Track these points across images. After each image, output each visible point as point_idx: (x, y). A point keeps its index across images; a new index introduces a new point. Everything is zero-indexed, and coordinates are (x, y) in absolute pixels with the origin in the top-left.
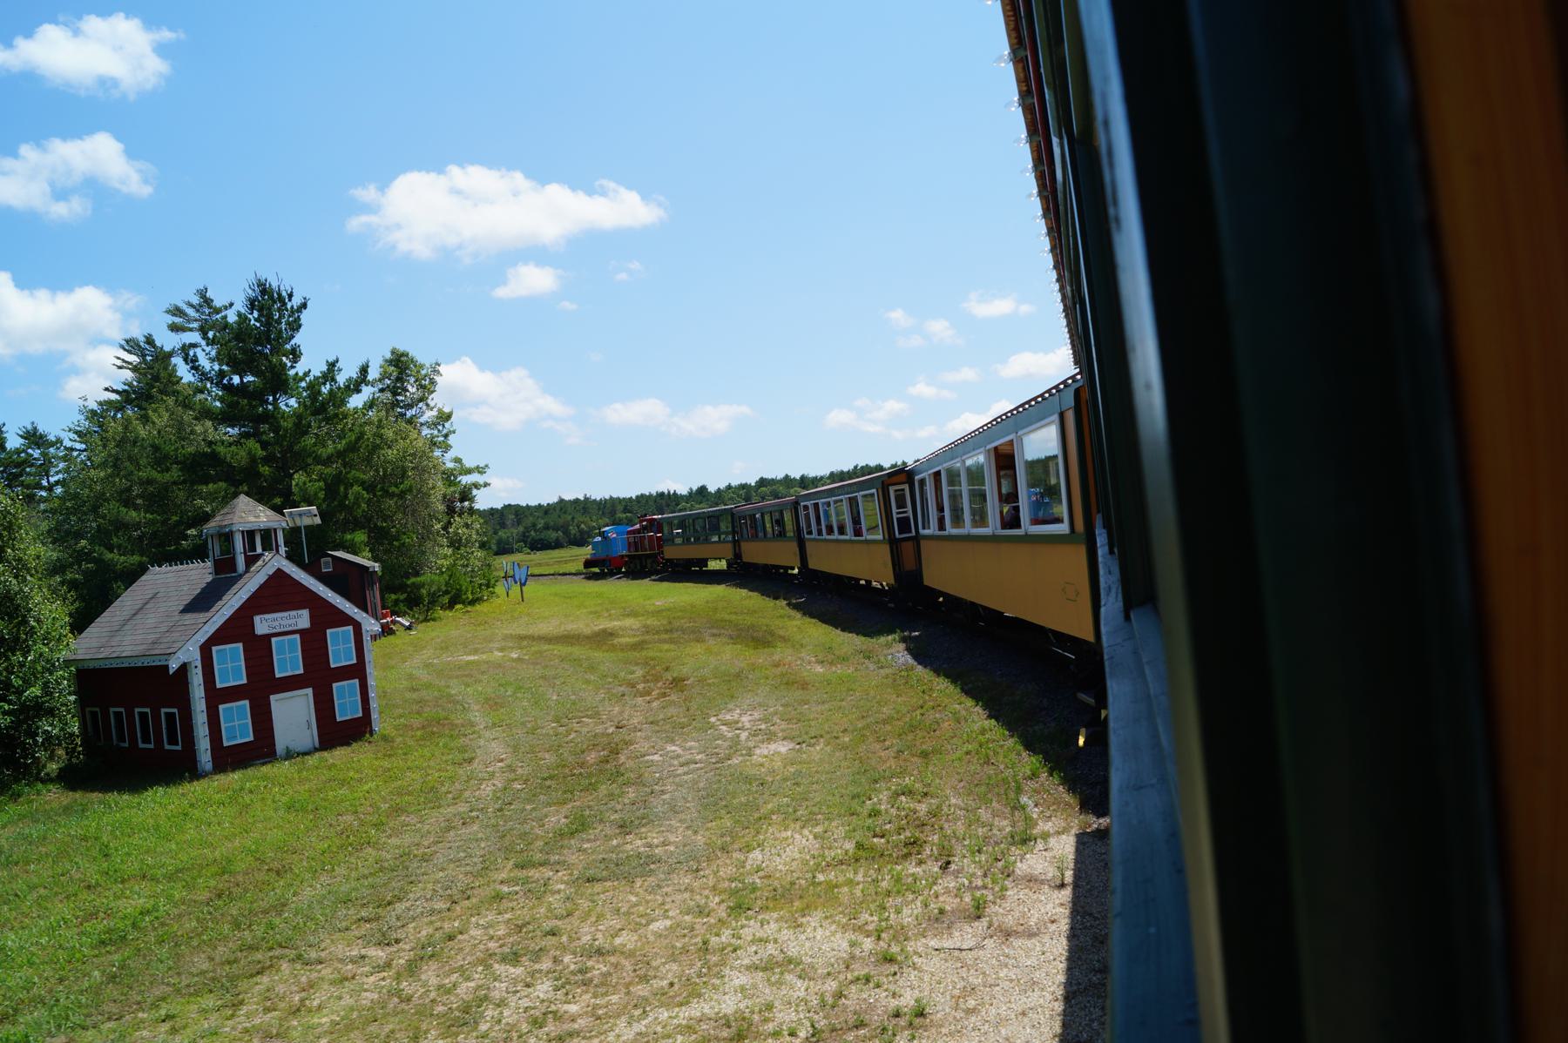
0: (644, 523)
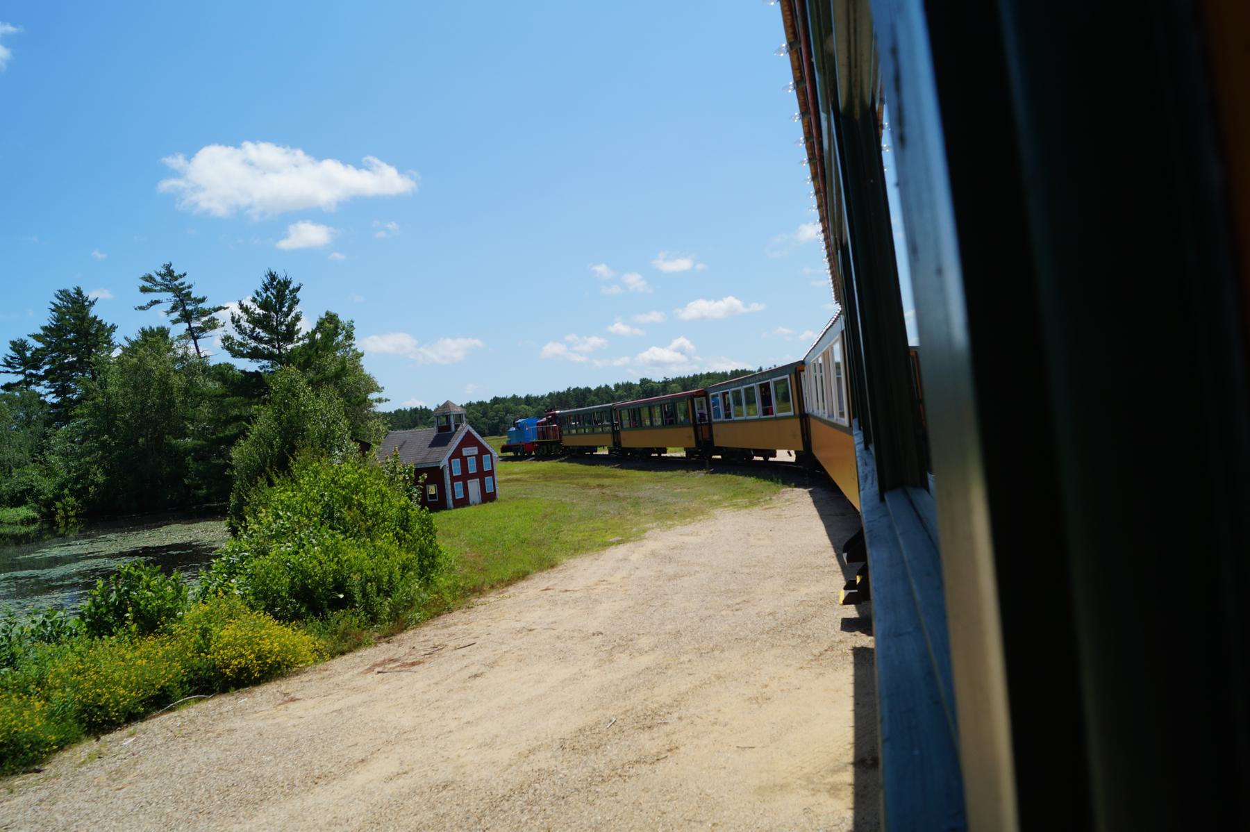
0: (550, 417)
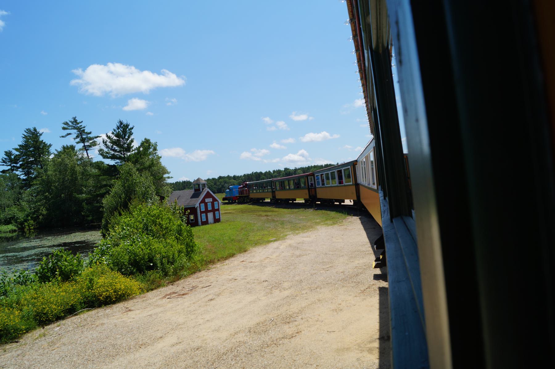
0: (244, 185)
